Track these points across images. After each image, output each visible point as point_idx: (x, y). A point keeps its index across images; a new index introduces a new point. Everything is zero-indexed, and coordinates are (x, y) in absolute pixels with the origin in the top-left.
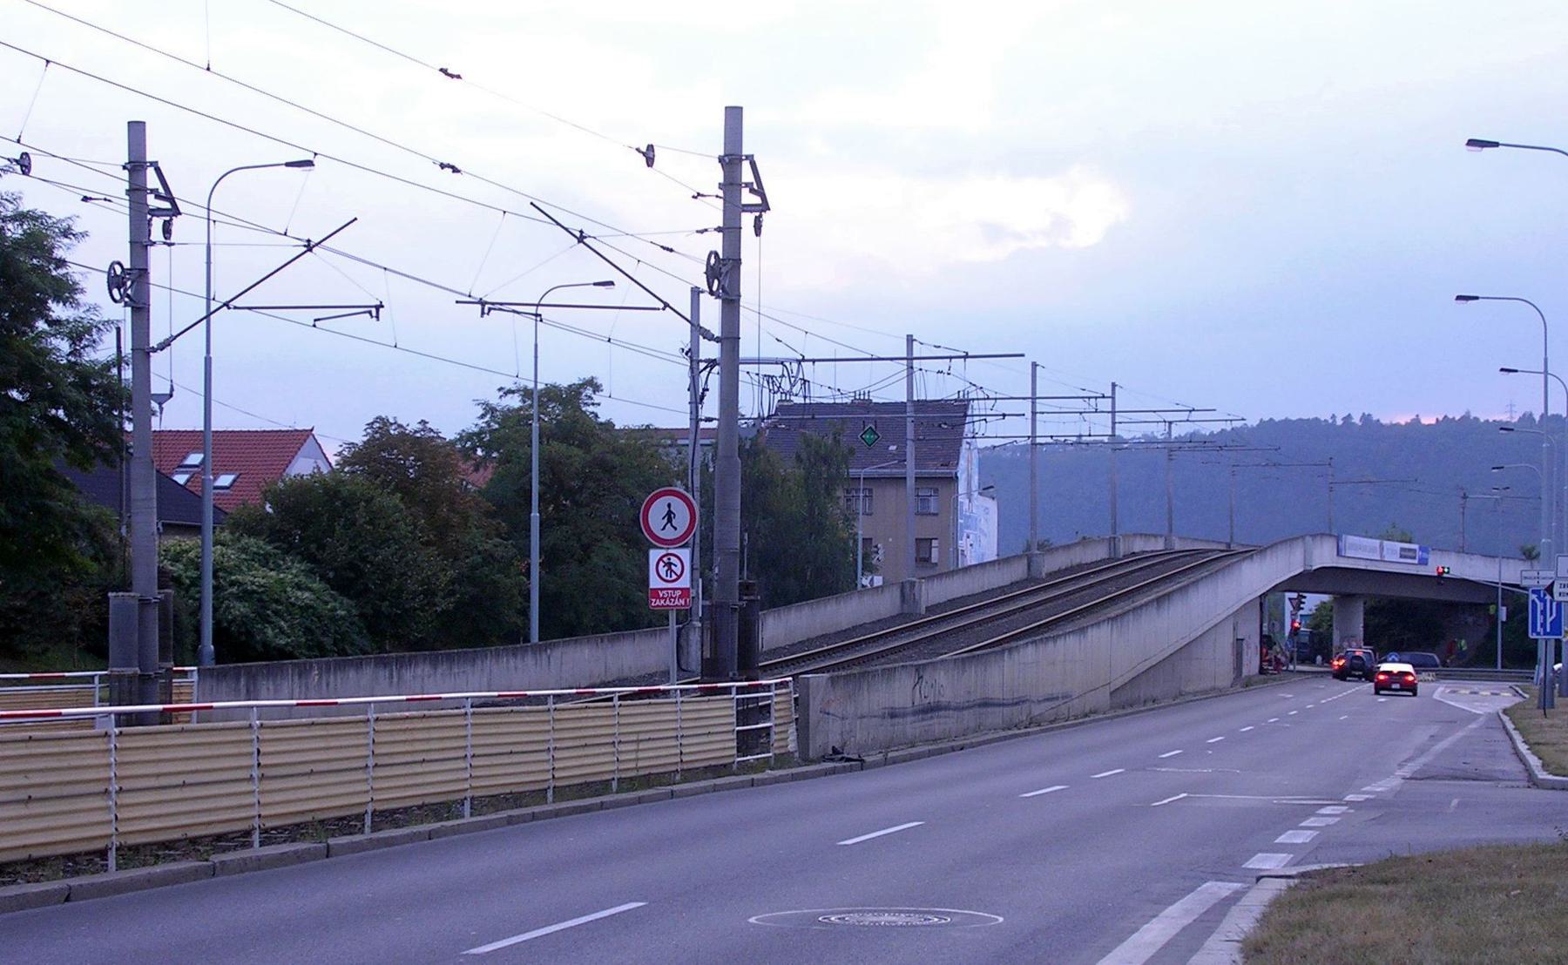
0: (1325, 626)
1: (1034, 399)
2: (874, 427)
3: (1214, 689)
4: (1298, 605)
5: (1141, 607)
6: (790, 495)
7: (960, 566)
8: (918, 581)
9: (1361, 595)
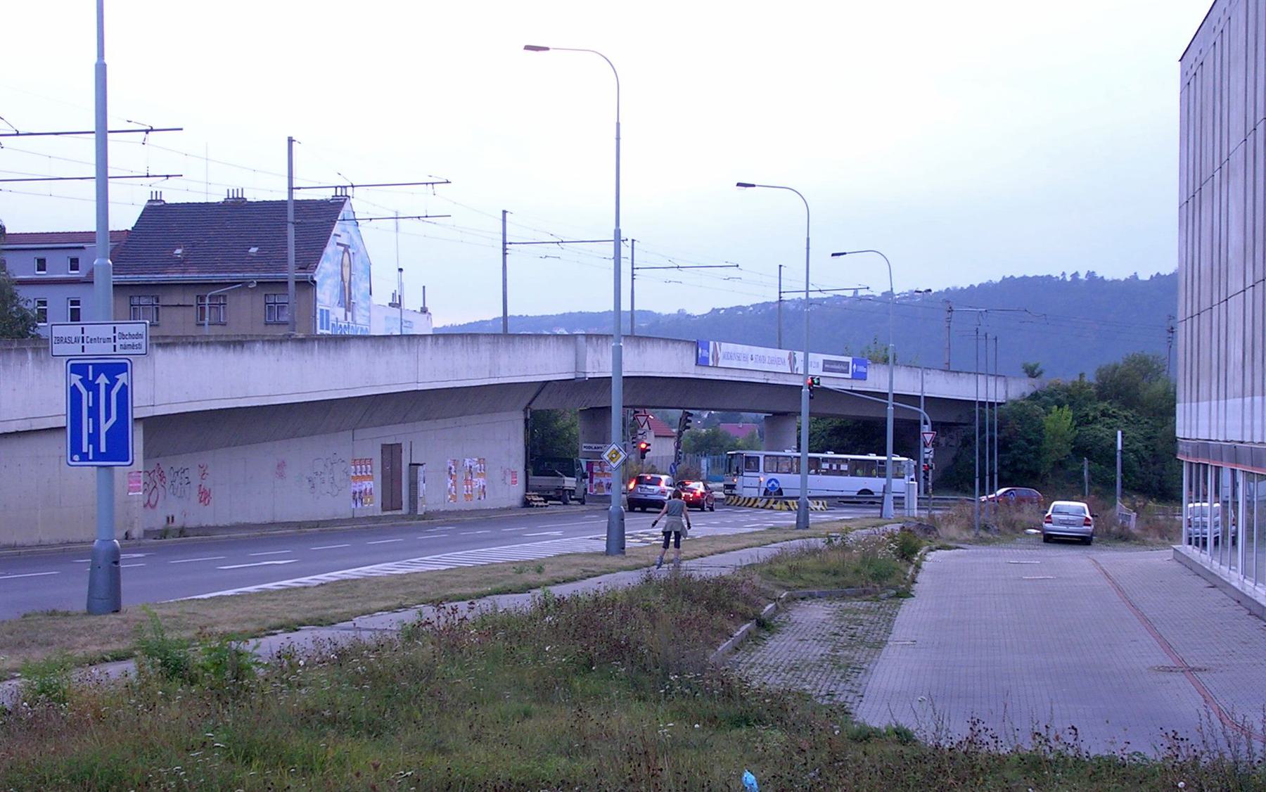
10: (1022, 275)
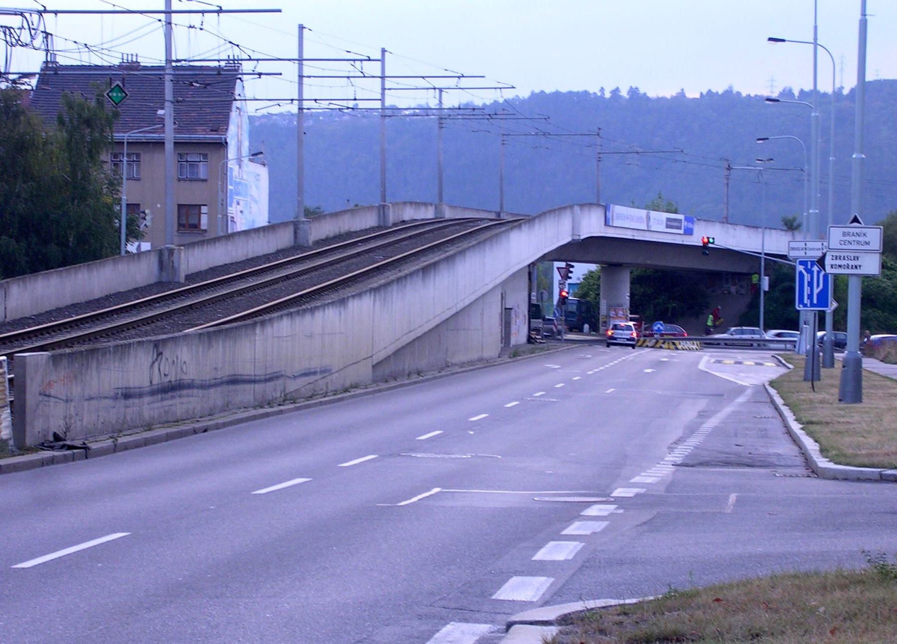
0: (592, 295)
1: (301, 60)
2: (121, 85)
3: (480, 360)
4: (566, 275)
5: (406, 277)
6: (51, 159)
7: (229, 232)
8: (176, 248)
9: (628, 265)
10: (553, 90)
